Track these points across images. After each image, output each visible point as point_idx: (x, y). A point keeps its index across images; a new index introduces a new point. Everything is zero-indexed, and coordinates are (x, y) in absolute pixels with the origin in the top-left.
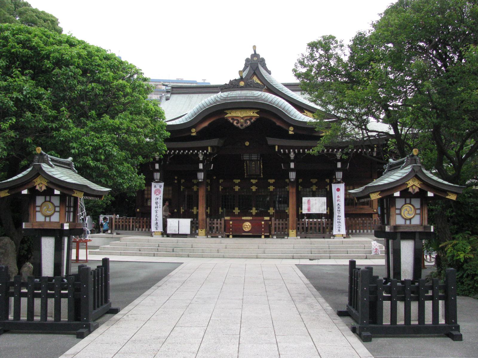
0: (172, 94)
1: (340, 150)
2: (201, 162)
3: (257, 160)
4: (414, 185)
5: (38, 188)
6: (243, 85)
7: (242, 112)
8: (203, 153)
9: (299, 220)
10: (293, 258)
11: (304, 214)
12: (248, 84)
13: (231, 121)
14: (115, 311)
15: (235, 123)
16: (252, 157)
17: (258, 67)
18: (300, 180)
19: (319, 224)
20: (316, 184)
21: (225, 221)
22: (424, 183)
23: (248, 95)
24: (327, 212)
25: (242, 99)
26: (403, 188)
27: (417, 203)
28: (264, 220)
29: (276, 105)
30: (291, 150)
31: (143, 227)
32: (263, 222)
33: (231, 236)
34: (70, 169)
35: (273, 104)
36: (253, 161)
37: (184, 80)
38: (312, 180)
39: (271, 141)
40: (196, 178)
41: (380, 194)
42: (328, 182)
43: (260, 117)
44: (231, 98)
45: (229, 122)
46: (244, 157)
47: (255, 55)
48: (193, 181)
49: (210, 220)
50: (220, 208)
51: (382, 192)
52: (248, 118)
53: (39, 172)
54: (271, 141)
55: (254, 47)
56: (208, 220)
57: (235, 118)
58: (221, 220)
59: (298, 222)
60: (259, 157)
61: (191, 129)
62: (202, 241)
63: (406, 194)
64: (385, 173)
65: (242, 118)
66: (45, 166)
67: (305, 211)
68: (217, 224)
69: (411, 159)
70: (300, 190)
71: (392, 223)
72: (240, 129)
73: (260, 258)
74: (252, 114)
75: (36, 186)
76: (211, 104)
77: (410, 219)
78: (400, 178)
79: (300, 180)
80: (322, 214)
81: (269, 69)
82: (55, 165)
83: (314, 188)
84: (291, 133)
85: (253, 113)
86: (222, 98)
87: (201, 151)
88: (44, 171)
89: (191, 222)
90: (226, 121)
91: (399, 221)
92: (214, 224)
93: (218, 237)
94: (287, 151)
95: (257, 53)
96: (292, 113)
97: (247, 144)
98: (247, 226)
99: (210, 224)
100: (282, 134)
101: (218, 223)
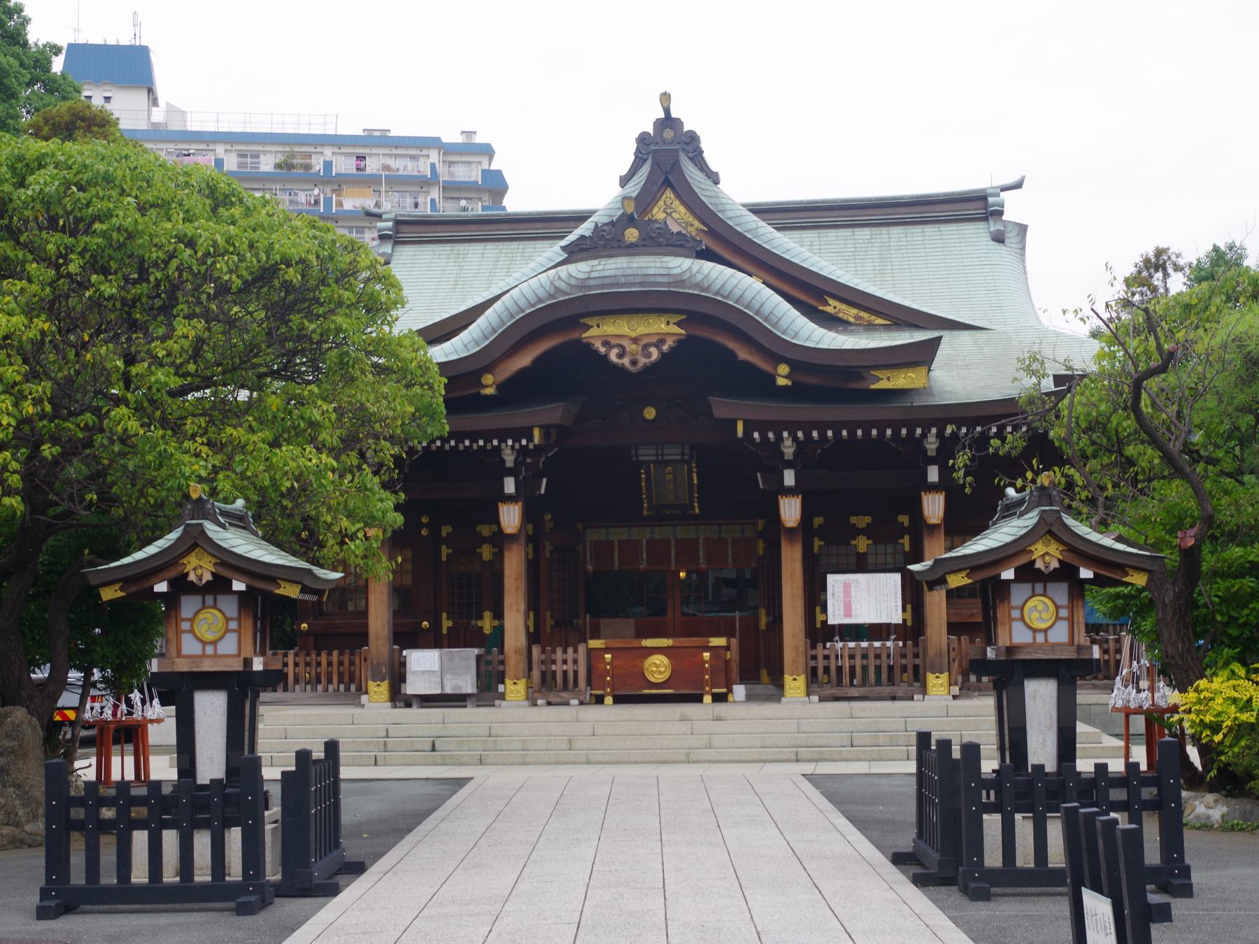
0: (397, 243)
1: (934, 431)
2: (510, 472)
3: (682, 461)
4: (1047, 555)
5: (192, 577)
6: (633, 240)
7: (634, 323)
8: (517, 446)
9: (814, 647)
10: (797, 761)
11: (833, 626)
12: (651, 238)
13: (602, 350)
14: (358, 868)
15: (613, 356)
16: (666, 451)
17: (676, 163)
18: (818, 521)
19: (878, 656)
20: (867, 532)
21: (590, 652)
22: (1071, 549)
23: (652, 271)
24: (904, 620)
25: (634, 284)
26: (1023, 560)
27: (1060, 592)
28: (707, 648)
29: (737, 302)
30: (785, 434)
31: (330, 681)
32: (706, 655)
33: (609, 700)
34: (244, 528)
35: (727, 297)
36: (667, 463)
37: (392, 134)
38: (853, 520)
39: (722, 408)
40: (495, 519)
41: (968, 576)
42: (906, 524)
43: (689, 337)
44: (599, 282)
45: (596, 352)
46: (641, 452)
47: (668, 122)
48: (479, 528)
49: (543, 652)
50: (444, 615)
51: (973, 570)
52: (654, 340)
53: (196, 541)
54: (722, 408)
55: (665, 98)
56: (536, 650)
57: (613, 341)
58: (576, 651)
59: (814, 653)
60: (687, 451)
61: (481, 376)
62: (516, 712)
63: (1028, 573)
64: (994, 523)
65: (635, 340)
66: (211, 528)
67: (835, 615)
68: (565, 662)
69: (1040, 496)
70: (816, 550)
71: (1003, 641)
72: (631, 374)
73: (698, 762)
74: (663, 328)
75: (187, 574)
76: (541, 301)
77: (1045, 631)
78: (1025, 531)
79: (818, 521)
80: (888, 625)
81: (713, 168)
82: (231, 524)
83: (862, 544)
84: (782, 382)
85: (668, 323)
86: (573, 282)
87: (510, 442)
88: (210, 540)
89: (479, 658)
90: (587, 347)
91: (1020, 635)
92: (554, 662)
93: (567, 704)
94: (771, 435)
95: (674, 115)
96: (784, 324)
97: (650, 413)
98: (658, 668)
99: (543, 662)
100: (762, 385)
101: (570, 660)
